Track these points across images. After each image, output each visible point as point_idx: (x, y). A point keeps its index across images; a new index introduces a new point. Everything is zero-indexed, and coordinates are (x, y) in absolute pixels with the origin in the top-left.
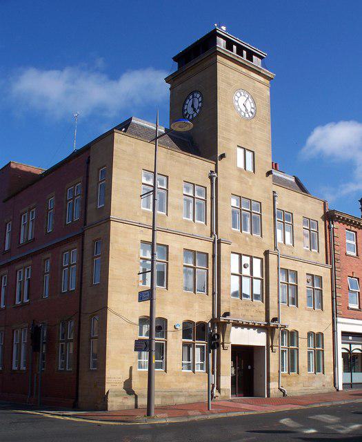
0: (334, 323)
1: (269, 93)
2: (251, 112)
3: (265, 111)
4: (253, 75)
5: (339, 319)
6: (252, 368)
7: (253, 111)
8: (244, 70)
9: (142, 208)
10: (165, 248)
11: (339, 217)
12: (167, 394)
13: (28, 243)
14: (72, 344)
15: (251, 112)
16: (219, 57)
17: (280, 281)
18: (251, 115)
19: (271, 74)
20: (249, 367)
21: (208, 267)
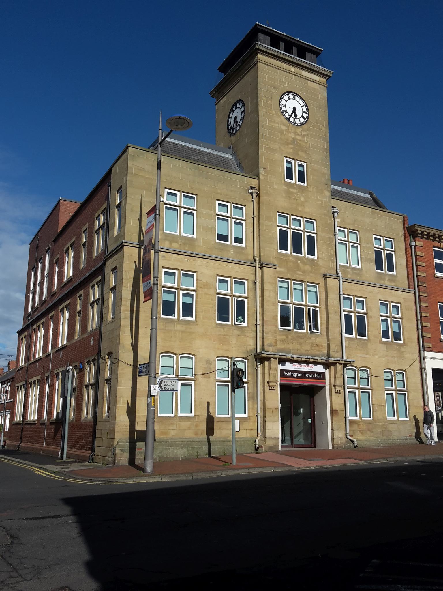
0: (421, 359)
1: (325, 94)
2: (302, 117)
3: (321, 115)
4: (305, 73)
5: (427, 354)
6: (313, 421)
7: (305, 115)
8: (293, 69)
9: (165, 231)
10: (391, 396)
11: (422, 232)
12: (281, 52)
13: (70, 280)
14: (86, 382)
15: (302, 117)
16: (259, 56)
17: (343, 308)
18: (302, 120)
19: (327, 71)
20: (310, 421)
21: (415, 289)
